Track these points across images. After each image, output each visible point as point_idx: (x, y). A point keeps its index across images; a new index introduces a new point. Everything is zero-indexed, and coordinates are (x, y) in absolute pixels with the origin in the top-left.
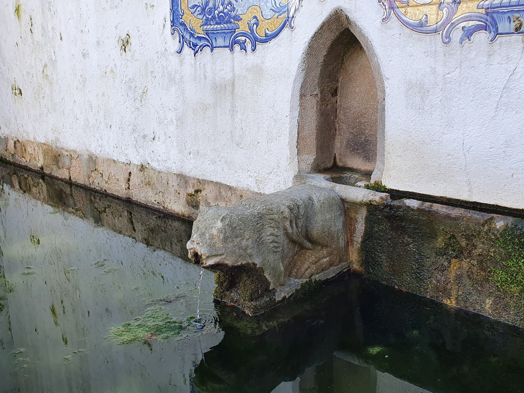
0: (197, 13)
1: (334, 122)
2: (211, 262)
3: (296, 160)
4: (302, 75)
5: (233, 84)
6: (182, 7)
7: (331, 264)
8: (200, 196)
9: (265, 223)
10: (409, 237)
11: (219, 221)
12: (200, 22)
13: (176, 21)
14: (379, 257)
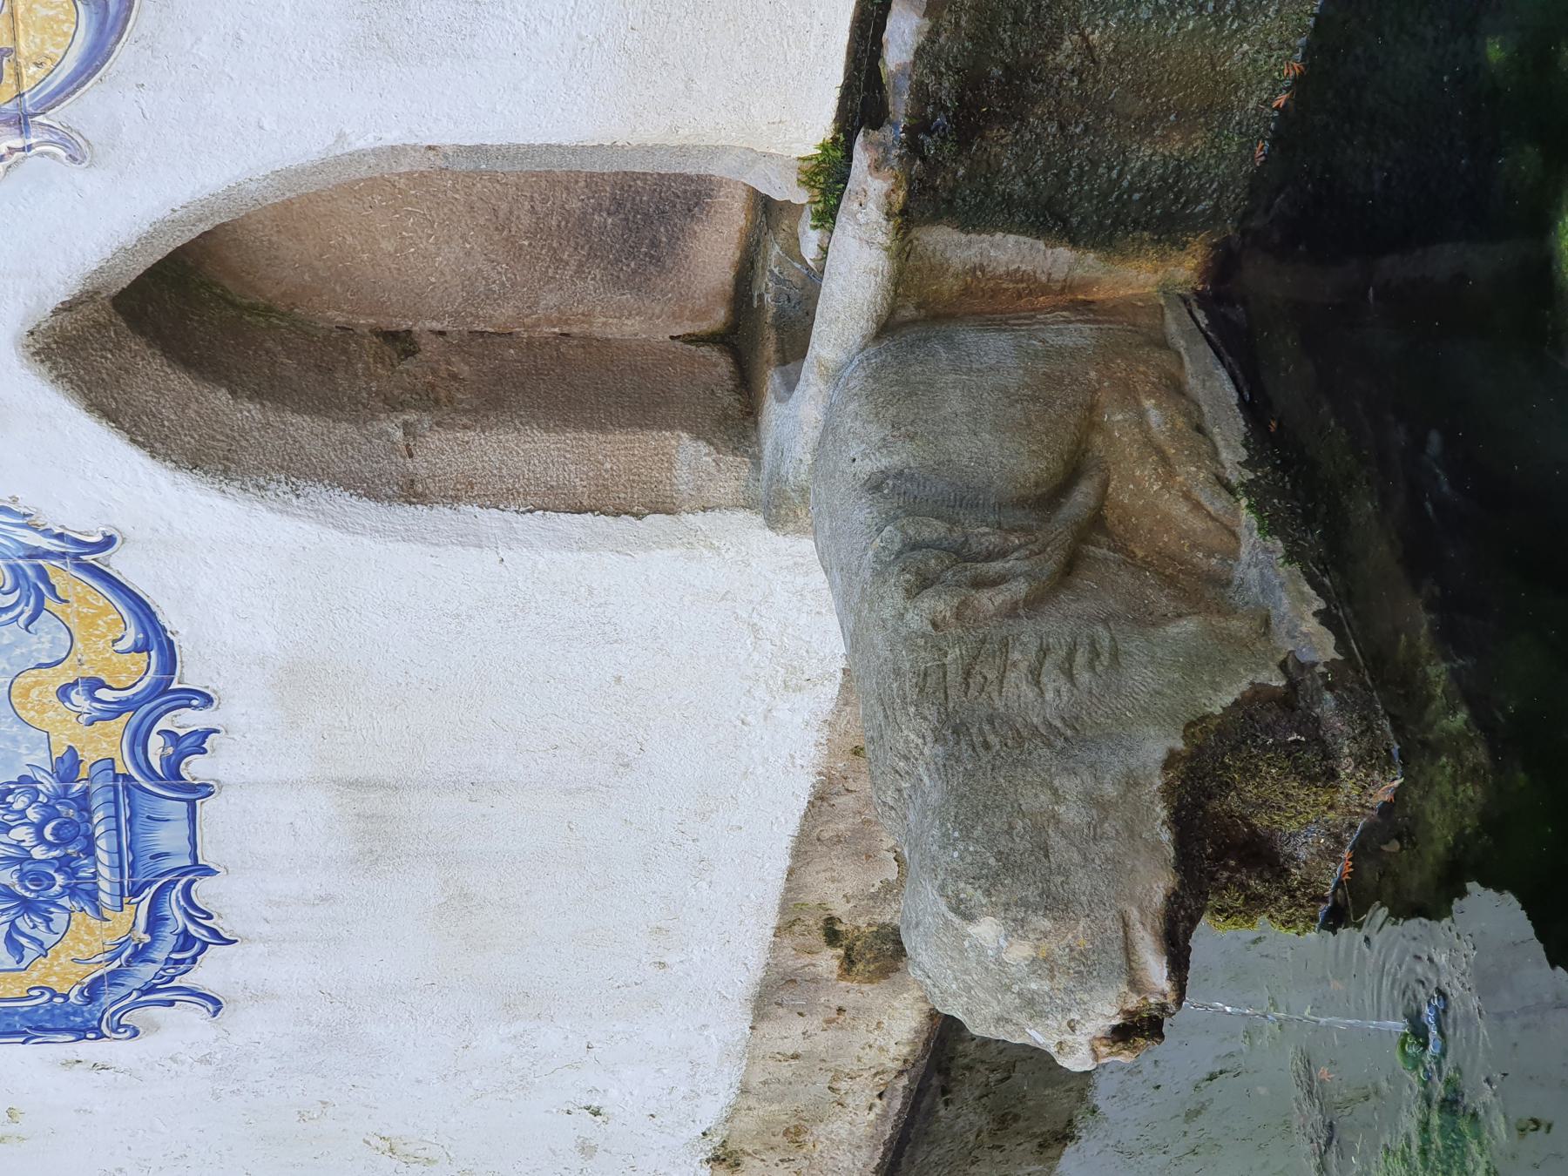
0: (41, 933)
1: (530, 343)
2: (1156, 971)
3: (698, 519)
4: (317, 493)
5: (355, 784)
6: (17, 993)
7: (1174, 388)
8: (853, 921)
9: (983, 712)
10: (1053, 44)
11: (972, 929)
12: (84, 919)
13: (76, 1018)
14: (1143, 171)
